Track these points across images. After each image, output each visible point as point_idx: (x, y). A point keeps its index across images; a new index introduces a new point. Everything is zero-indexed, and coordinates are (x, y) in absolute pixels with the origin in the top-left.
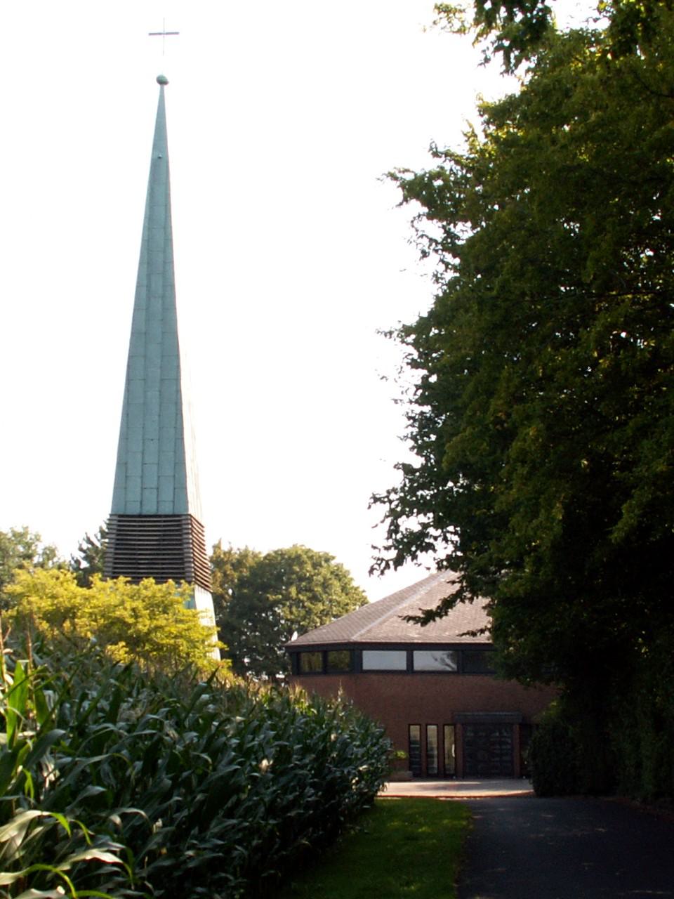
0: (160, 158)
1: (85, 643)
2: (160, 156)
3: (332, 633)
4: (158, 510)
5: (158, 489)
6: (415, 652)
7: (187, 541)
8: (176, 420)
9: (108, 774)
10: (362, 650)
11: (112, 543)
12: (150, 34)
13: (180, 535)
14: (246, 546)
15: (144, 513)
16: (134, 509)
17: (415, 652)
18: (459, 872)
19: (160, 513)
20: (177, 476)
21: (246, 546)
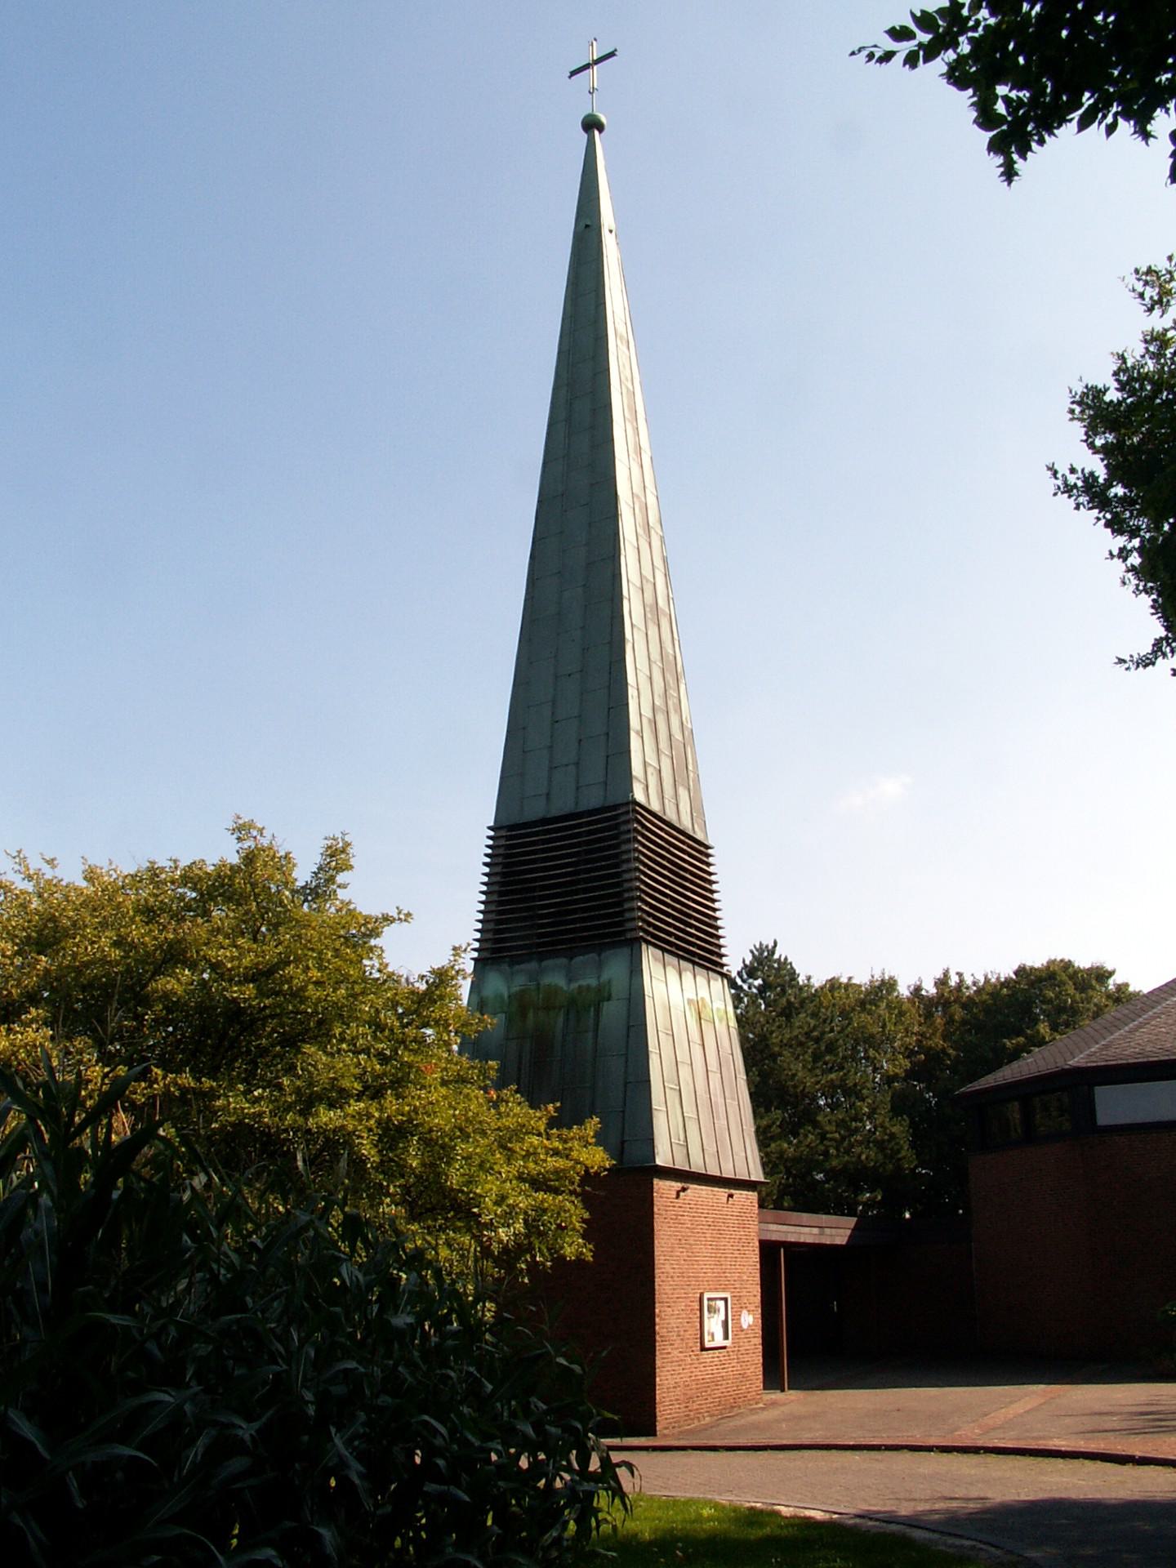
0: (587, 226)
1: (303, 1334)
2: (588, 223)
3: (1098, 1027)
4: (577, 803)
5: (577, 764)
6: (1098, 1089)
7: (631, 894)
8: (613, 584)
9: (616, 829)
10: (1091, 1086)
11: (492, 912)
12: (573, 73)
13: (618, 885)
14: (1147, 144)
15: (555, 812)
16: (535, 810)
17: (1098, 1089)
18: (239, 904)
19: (581, 809)
20: (611, 734)
21: (1147, 144)
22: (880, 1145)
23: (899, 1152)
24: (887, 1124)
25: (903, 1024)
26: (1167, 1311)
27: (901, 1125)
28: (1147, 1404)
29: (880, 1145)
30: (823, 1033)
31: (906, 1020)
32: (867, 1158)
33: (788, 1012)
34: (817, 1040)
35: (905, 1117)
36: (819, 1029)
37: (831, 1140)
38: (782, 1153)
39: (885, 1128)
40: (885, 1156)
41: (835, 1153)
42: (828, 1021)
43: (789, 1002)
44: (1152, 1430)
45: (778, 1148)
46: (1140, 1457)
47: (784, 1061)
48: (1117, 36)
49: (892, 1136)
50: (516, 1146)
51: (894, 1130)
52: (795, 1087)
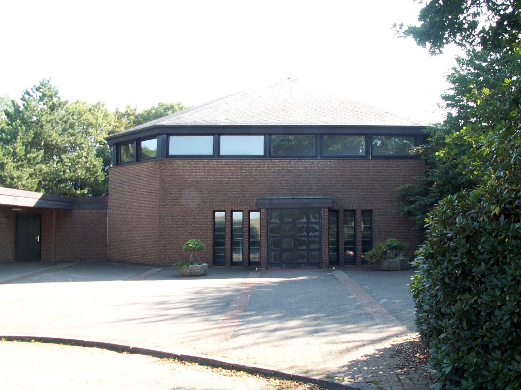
22: (88, 169)
23: (96, 173)
24: (93, 160)
25: (107, 120)
26: (188, 244)
27: (99, 161)
28: (163, 296)
29: (88, 169)
30: (69, 119)
31: (109, 118)
32: (81, 174)
33: (52, 108)
34: (66, 122)
35: (101, 157)
36: (67, 117)
37: (66, 166)
38: (41, 170)
39: (91, 162)
40: (90, 174)
41: (69, 171)
42: (71, 114)
43: (53, 103)
44: (153, 319)
45: (40, 167)
46: (133, 348)
47: (46, 129)
48: (518, 313)
49: (95, 166)
50: (464, 41)
51: (95, 163)
52: (52, 141)
